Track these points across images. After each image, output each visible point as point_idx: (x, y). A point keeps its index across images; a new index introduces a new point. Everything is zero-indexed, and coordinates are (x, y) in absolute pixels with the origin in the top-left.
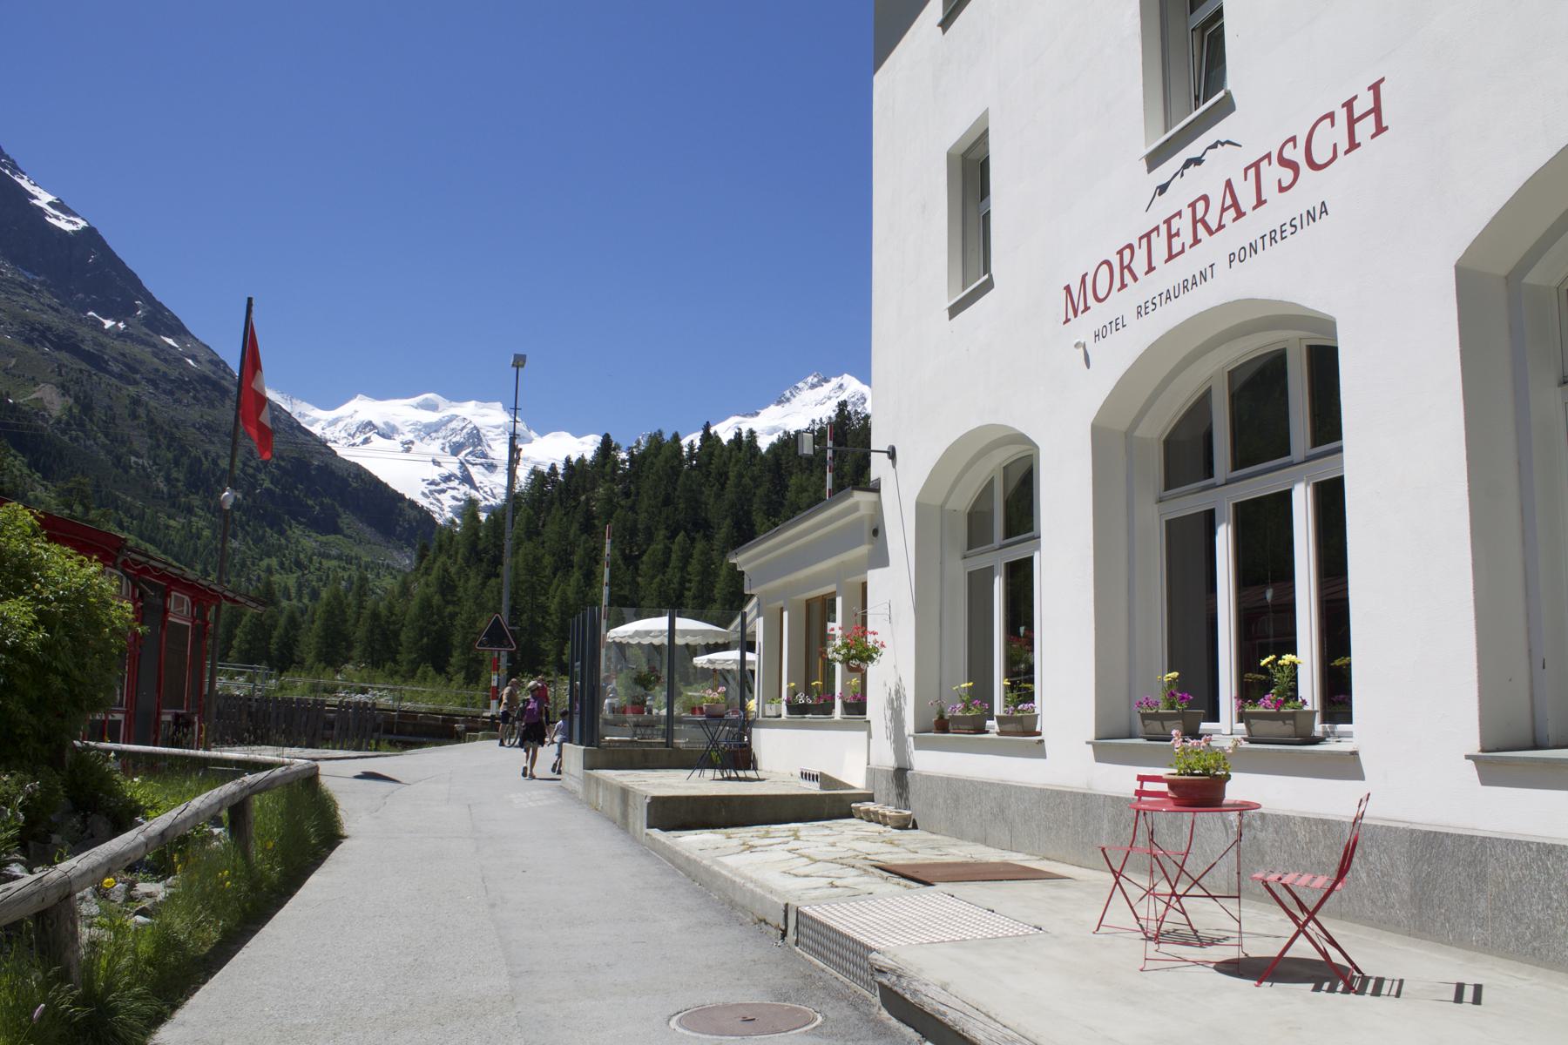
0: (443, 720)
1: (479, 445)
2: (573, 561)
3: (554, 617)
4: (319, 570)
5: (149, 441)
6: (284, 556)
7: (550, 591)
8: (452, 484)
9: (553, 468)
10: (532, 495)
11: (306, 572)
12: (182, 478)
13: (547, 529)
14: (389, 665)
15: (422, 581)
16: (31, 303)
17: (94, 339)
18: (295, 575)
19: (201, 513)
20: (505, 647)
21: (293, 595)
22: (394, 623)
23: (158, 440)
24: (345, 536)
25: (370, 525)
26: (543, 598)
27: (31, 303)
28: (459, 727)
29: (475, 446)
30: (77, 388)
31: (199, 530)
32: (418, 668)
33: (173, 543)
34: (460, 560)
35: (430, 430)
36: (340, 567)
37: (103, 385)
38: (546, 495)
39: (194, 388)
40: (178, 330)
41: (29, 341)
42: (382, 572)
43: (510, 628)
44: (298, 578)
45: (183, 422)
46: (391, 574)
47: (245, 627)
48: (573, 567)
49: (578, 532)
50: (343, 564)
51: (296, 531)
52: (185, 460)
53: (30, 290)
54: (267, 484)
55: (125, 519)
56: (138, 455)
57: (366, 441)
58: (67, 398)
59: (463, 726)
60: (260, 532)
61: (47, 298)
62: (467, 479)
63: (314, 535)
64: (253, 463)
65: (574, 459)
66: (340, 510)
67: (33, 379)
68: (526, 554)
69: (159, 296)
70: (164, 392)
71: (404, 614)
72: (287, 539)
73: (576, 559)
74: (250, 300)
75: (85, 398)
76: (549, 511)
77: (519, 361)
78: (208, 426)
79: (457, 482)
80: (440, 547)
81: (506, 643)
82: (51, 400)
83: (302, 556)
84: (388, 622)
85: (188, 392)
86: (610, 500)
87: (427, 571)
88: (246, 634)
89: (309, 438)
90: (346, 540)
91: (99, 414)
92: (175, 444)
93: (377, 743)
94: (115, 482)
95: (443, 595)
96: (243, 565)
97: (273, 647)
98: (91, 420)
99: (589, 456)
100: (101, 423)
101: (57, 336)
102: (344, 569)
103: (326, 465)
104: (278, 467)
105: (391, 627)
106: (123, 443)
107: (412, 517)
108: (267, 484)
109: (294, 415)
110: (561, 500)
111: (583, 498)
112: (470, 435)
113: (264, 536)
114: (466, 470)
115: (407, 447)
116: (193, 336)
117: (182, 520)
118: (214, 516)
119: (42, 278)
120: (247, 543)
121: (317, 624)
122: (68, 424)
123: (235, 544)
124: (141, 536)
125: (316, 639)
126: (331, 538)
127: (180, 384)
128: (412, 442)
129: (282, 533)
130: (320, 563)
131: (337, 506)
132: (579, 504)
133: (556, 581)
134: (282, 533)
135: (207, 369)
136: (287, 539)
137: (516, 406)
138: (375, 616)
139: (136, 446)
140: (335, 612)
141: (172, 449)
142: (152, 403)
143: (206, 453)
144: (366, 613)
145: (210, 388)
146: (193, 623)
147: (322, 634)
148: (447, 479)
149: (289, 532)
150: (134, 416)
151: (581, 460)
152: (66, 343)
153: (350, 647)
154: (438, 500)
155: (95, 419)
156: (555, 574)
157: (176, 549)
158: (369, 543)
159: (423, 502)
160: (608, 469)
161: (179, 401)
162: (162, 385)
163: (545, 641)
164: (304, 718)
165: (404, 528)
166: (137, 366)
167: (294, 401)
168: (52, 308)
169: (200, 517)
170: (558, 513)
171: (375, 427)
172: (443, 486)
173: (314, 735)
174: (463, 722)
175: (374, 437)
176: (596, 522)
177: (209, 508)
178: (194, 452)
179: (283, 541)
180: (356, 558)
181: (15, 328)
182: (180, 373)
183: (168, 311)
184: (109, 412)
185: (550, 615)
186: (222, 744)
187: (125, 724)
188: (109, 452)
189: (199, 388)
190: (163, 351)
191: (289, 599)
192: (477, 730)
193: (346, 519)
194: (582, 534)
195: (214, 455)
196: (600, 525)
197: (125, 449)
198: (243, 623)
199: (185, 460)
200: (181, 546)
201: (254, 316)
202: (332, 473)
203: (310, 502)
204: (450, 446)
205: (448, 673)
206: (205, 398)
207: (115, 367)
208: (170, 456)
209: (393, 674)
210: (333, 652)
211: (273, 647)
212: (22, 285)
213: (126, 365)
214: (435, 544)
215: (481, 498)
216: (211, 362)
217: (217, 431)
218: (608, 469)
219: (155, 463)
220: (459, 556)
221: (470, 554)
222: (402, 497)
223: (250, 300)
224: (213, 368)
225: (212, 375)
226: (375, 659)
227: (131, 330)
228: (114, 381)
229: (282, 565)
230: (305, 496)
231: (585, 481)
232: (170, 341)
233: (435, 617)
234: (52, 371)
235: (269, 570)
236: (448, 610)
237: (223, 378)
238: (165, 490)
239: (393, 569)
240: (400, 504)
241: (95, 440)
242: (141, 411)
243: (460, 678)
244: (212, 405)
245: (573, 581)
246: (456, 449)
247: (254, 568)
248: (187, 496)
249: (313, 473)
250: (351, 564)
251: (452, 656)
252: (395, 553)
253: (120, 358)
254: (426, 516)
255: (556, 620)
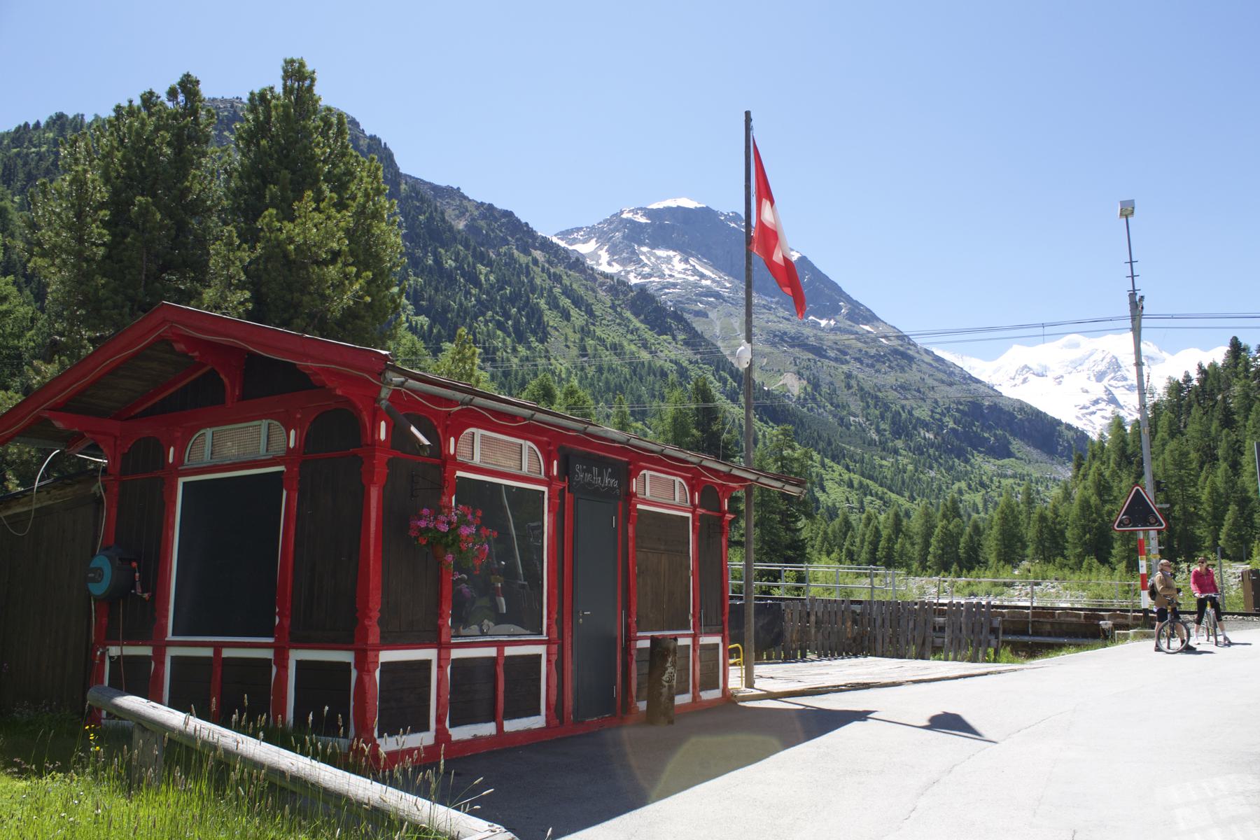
0: (1086, 616)
1: (1119, 371)
2: (1218, 455)
3: (1205, 506)
4: (999, 487)
5: (861, 404)
6: (971, 479)
7: (1199, 483)
8: (1099, 406)
9: (1188, 379)
10: (1170, 401)
11: (989, 490)
12: (888, 428)
13: (1189, 429)
14: (1058, 559)
15: (1081, 486)
16: (772, 317)
17: (815, 336)
18: (981, 493)
19: (904, 453)
20: (1152, 525)
21: (981, 509)
22: (1059, 523)
23: (867, 402)
24: (1017, 458)
25: (1036, 447)
26: (1193, 489)
27: (772, 317)
28: (1106, 624)
29: (1116, 372)
30: (808, 373)
31: (905, 466)
32: (1083, 560)
33: (886, 478)
34: (1112, 464)
35: (1076, 365)
36: (1015, 484)
37: (825, 368)
38: (1183, 400)
39: (889, 360)
40: (871, 318)
41: (774, 344)
42: (1050, 485)
43: (1157, 506)
44: (983, 495)
45: (884, 386)
46: (1058, 485)
47: (937, 536)
48: (1218, 460)
49: (1220, 428)
50: (1018, 481)
51: (977, 458)
52: (888, 415)
53: (770, 309)
54: (951, 425)
55: (850, 464)
56: (855, 416)
57: (1025, 381)
58: (802, 381)
59: (1109, 622)
60: (951, 463)
61: (782, 312)
62: (1113, 400)
63: (992, 460)
64: (939, 410)
65: (1206, 366)
66: (1011, 438)
67: (779, 371)
68: (1172, 451)
69: (855, 296)
70: (867, 365)
71: (1067, 515)
72: (972, 466)
73: (1220, 452)
74: (748, 114)
75: (814, 379)
76: (1189, 413)
77: (1127, 211)
78: (902, 387)
79: (1104, 403)
80: (1094, 456)
81: (1152, 520)
82: (792, 385)
83: (984, 478)
84: (1053, 523)
85: (884, 363)
86: (1247, 396)
87: (1085, 476)
88: (938, 542)
89: (979, 385)
90: (1018, 462)
91: (825, 389)
92: (880, 404)
93: (996, 652)
94: (841, 437)
95: (1100, 495)
96: (940, 489)
97: (961, 551)
98: (820, 394)
99: (1220, 362)
100: (827, 396)
101: (791, 338)
102: (1019, 485)
103: (995, 404)
104: (958, 410)
105: (1058, 527)
106: (844, 407)
107: (1069, 437)
108: (951, 425)
109: (965, 369)
110: (1198, 401)
111: (1220, 397)
112: (1110, 363)
113: (954, 465)
114: (1110, 393)
115: (1059, 379)
116: (883, 322)
117: (891, 460)
118: (914, 454)
119: (776, 299)
120: (941, 472)
121: (996, 529)
122: (805, 399)
123: (932, 474)
124: (863, 475)
125: (995, 542)
126: (1006, 461)
127: (879, 358)
128: (1062, 377)
129: (967, 461)
130: (999, 482)
131: (1008, 435)
132: (1216, 403)
133: (1203, 474)
134: (967, 461)
135: (895, 343)
136: (972, 466)
137: (1132, 273)
138: (1043, 518)
139: (853, 408)
140: (1010, 520)
141: (878, 407)
142: (861, 376)
143: (903, 407)
144: (1035, 516)
145: (899, 357)
146: (693, 513)
147: (1000, 537)
148: (1096, 402)
149: (973, 460)
150: (849, 387)
151: (1213, 365)
152: (797, 342)
153: (1024, 546)
154: (1091, 421)
155: (823, 393)
156: (1201, 468)
157: (889, 482)
158: (1037, 462)
159: (1076, 424)
160: (1240, 368)
161: (878, 371)
162: (866, 361)
163: (1199, 529)
164: (911, 624)
165: (1064, 447)
166: (847, 350)
167: (964, 358)
168: (785, 319)
169: (905, 456)
170: (1196, 412)
171: (1030, 369)
172: (1093, 409)
173: (924, 643)
174: (1110, 618)
175: (1031, 377)
176: (1236, 417)
177: (910, 448)
178: (894, 408)
179: (969, 468)
180: (1028, 475)
181: (764, 337)
182: (877, 350)
183: (863, 306)
184: (831, 386)
185: (1202, 504)
186: (833, 656)
187: (548, 661)
188: (835, 416)
189: (892, 359)
190: (862, 335)
191: (978, 513)
192: (1127, 627)
193: (1016, 445)
194: (1224, 428)
195: (909, 408)
196: (1240, 419)
197: (845, 413)
198: (936, 533)
199: (888, 415)
200: (892, 480)
201: (755, 133)
202: (1001, 409)
203: (986, 435)
204: (1095, 375)
205: (1111, 563)
206: (897, 365)
207: (831, 354)
208: (877, 412)
209: (1062, 566)
210: (1011, 553)
211: (961, 551)
212: (764, 306)
213: (839, 350)
214: (1089, 454)
215: (1127, 415)
216: (898, 337)
217: (909, 390)
218: (1240, 368)
219: (868, 420)
220: (1111, 461)
221: (1121, 458)
222: (1059, 423)
223: (748, 114)
224: (900, 342)
225: (900, 348)
226: (1046, 555)
227: (839, 325)
228: (832, 363)
229: (969, 486)
230: (982, 430)
231: (1219, 381)
232: (867, 328)
233: (1094, 515)
234: (791, 363)
235: (960, 492)
236: (1106, 508)
237: (909, 349)
238: (877, 438)
239: (1059, 481)
240: (1058, 428)
241: (824, 408)
242: (853, 383)
243: (1122, 566)
244: (903, 370)
245: (1220, 472)
246: (1100, 377)
247: (949, 491)
248: (893, 441)
249: (986, 411)
250: (1024, 480)
251: (1113, 548)
252: (1059, 468)
253: (835, 346)
254: (1082, 437)
255: (1208, 509)
